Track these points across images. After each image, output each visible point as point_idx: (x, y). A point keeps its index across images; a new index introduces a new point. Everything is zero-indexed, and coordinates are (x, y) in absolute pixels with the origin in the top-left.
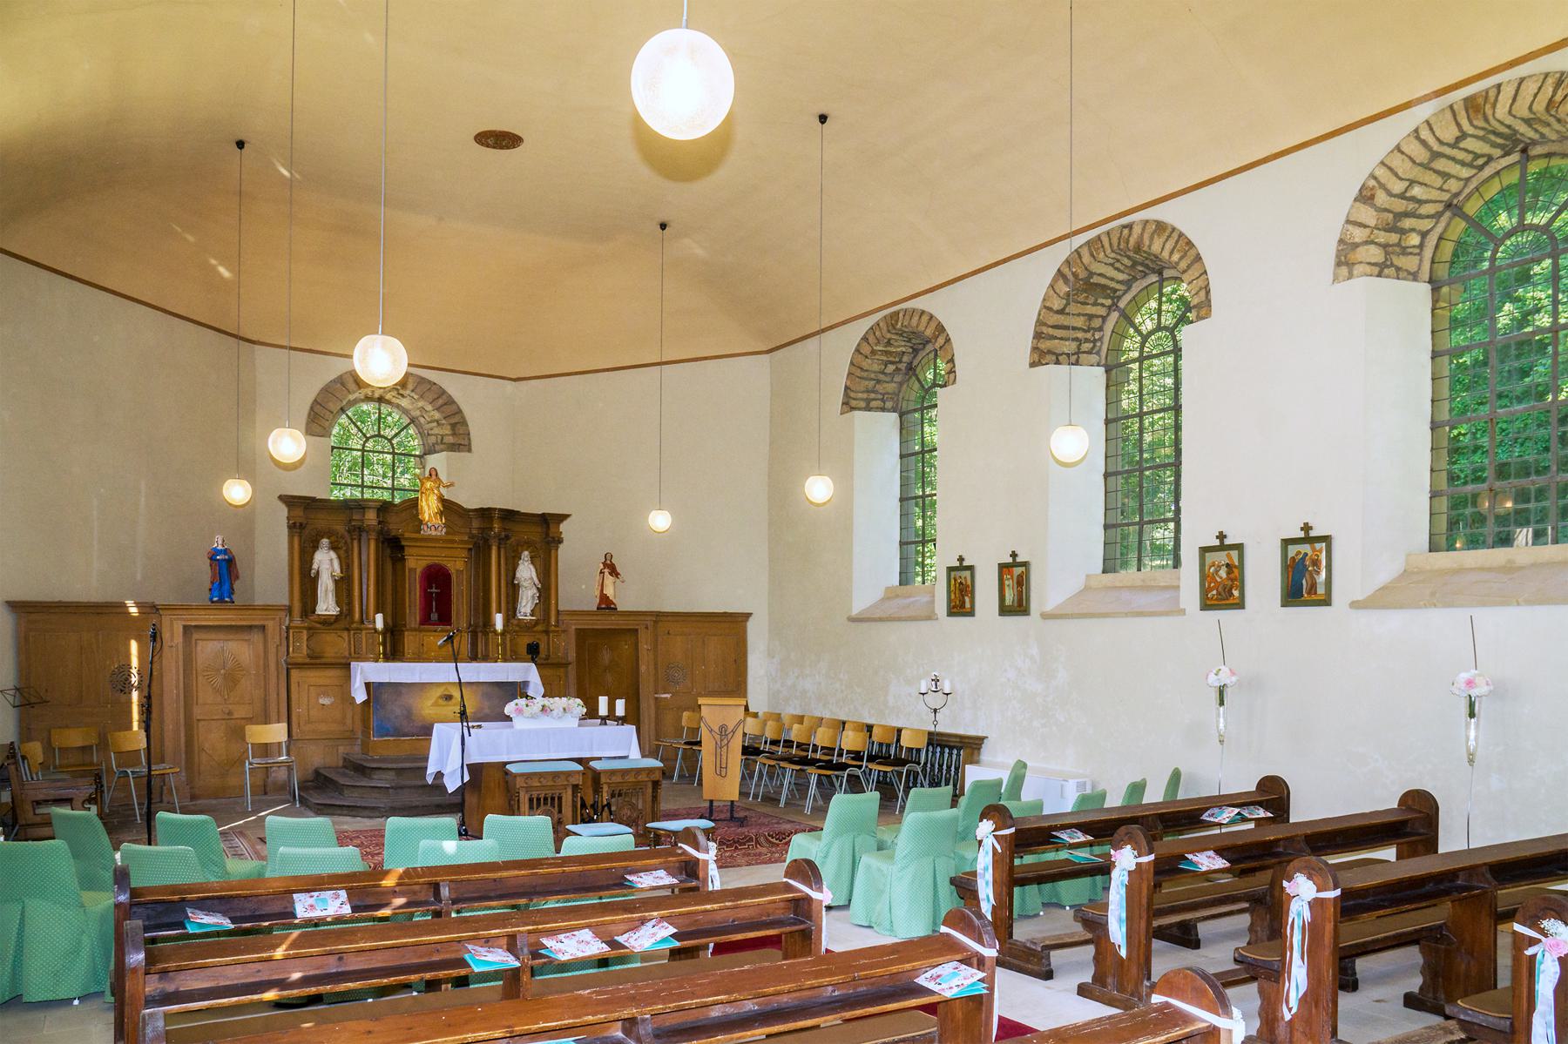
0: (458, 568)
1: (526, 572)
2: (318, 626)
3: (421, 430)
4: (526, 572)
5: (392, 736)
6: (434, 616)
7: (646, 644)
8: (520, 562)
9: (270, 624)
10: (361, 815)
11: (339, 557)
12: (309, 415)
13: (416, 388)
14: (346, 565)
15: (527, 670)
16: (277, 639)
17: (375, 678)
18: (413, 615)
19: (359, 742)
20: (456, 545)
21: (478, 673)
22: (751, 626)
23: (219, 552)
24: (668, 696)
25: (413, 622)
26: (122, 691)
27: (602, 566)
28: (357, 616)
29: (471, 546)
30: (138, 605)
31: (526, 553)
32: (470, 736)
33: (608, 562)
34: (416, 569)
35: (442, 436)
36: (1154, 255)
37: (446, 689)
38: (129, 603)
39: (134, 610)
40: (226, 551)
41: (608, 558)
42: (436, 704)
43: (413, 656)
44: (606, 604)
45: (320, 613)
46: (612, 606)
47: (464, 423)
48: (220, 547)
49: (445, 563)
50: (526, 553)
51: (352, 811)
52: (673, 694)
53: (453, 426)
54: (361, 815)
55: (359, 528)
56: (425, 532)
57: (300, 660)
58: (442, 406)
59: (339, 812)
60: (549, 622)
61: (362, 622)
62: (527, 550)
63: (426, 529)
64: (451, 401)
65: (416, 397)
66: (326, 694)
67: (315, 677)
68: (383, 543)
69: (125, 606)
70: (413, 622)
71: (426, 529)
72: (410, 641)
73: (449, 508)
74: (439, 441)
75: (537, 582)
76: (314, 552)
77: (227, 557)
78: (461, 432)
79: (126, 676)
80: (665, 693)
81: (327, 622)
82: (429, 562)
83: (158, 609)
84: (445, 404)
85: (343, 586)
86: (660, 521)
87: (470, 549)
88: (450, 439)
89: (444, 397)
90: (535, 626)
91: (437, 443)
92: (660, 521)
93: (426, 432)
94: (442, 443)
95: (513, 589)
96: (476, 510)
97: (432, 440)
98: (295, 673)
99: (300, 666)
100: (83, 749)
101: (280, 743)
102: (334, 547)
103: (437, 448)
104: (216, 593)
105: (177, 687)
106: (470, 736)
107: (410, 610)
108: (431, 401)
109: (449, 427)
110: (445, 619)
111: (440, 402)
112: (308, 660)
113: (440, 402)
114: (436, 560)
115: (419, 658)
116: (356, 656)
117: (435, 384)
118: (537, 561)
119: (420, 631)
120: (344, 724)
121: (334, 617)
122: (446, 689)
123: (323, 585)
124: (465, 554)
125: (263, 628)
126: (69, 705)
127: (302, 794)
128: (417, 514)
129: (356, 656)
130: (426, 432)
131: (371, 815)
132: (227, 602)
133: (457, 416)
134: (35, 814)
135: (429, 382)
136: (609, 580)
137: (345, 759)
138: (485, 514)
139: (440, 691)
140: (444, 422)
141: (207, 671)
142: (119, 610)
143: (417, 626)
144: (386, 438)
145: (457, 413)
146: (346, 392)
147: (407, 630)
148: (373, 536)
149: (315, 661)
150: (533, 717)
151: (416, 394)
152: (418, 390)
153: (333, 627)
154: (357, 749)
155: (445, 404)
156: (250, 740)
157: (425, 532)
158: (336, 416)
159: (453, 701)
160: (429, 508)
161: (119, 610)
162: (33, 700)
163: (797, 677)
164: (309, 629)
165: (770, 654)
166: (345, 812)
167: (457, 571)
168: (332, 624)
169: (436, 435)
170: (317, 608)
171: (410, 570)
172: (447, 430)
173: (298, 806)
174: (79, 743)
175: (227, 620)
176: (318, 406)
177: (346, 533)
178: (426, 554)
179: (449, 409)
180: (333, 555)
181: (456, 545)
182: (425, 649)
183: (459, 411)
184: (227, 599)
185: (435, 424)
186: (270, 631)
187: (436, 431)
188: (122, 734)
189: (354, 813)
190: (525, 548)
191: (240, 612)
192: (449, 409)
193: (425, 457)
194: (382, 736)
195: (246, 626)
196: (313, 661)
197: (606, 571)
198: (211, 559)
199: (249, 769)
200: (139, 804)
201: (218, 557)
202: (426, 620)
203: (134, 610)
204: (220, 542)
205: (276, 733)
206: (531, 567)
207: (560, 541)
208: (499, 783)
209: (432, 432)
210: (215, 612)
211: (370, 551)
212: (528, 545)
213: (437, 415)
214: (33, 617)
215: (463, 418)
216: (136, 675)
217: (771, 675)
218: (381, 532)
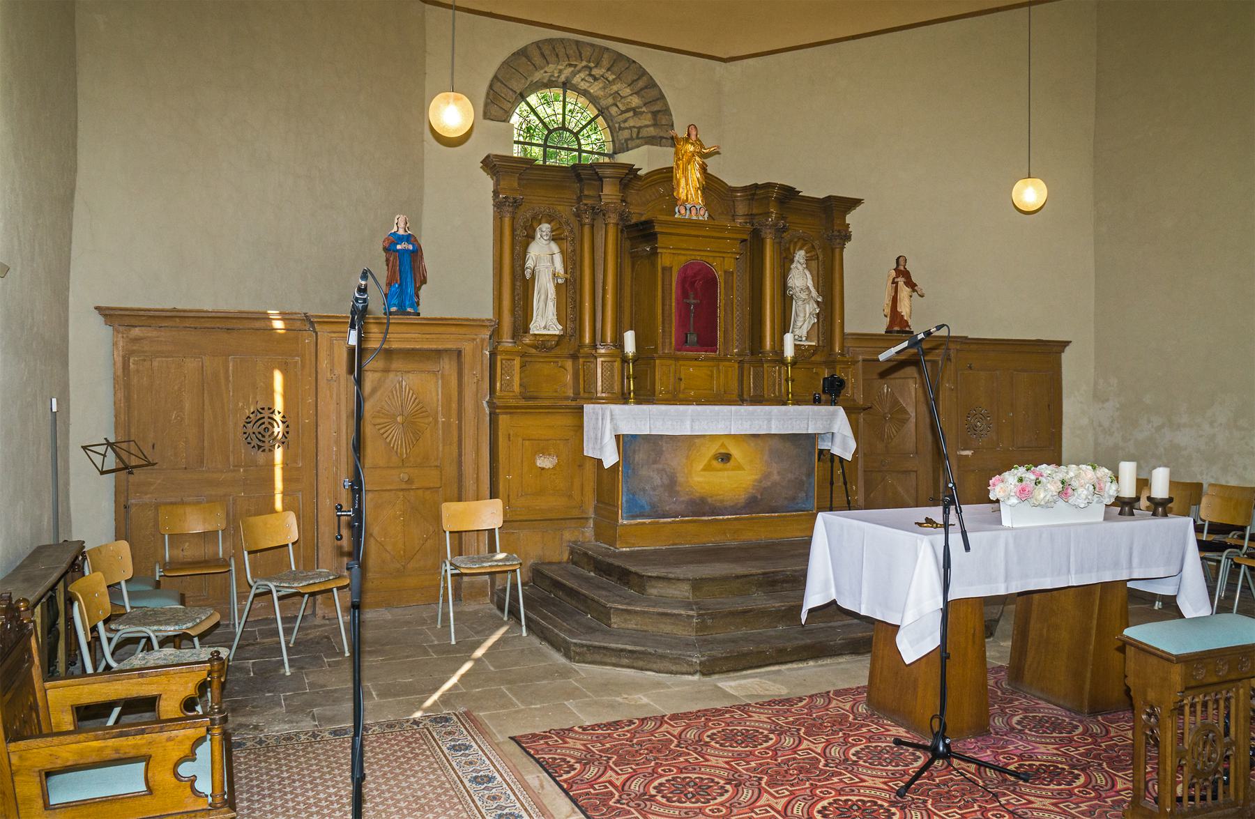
0: (726, 268)
1: (801, 279)
2: (534, 351)
3: (611, 124)
4: (801, 279)
5: (649, 517)
6: (693, 338)
7: (948, 382)
8: (793, 266)
9: (467, 348)
10: (654, 666)
11: (562, 252)
12: (488, 94)
13: (612, 66)
14: (572, 261)
15: (833, 416)
16: (477, 371)
17: (627, 429)
18: (667, 331)
19: (591, 523)
20: (726, 234)
21: (769, 420)
22: (1067, 357)
23: (401, 239)
24: (968, 453)
25: (667, 347)
26: (259, 447)
27: (893, 273)
28: (587, 340)
29: (745, 237)
30: (285, 317)
31: (802, 253)
32: (967, 548)
33: (902, 268)
34: (671, 268)
35: (639, 128)
36: (488, 320)
37: (723, 445)
38: (273, 312)
39: (278, 324)
40: (408, 238)
41: (901, 262)
42: (708, 468)
43: (667, 396)
44: (898, 326)
45: (536, 332)
46: (907, 329)
47: (667, 111)
48: (401, 232)
49: (710, 260)
50: (802, 253)
51: (637, 658)
52: (976, 451)
53: (655, 114)
54: (654, 666)
55: (593, 208)
56: (681, 213)
57: (513, 402)
58: (642, 89)
59: (614, 660)
60: (832, 349)
61: (594, 347)
62: (801, 249)
63: (683, 211)
64: (652, 84)
65: (611, 78)
66: (544, 452)
67: (536, 426)
68: (622, 231)
69: (266, 318)
70: (667, 347)
71: (683, 211)
72: (662, 374)
73: (711, 186)
74: (634, 136)
75: (814, 293)
76: (528, 245)
77: (411, 247)
78: (664, 122)
79: (266, 425)
80: (965, 449)
81: (544, 344)
82: (689, 258)
83: (312, 323)
84: (646, 87)
85: (569, 292)
86: (1030, 194)
87: (744, 241)
88: (652, 131)
89: (645, 78)
90: (813, 354)
91: (631, 139)
92: (1030, 194)
93: (617, 125)
94: (638, 138)
95: (785, 300)
96: (745, 189)
97: (625, 134)
98: (503, 420)
99: (511, 410)
100: (204, 536)
101: (492, 531)
102: (555, 239)
103: (630, 144)
104: (395, 301)
105: (337, 443)
106: (967, 548)
107: (663, 327)
108: (630, 81)
109: (649, 115)
110: (708, 342)
111: (641, 84)
112: (523, 403)
113: (641, 84)
114: (698, 257)
115: (674, 398)
116: (586, 395)
117: (634, 62)
118: (814, 264)
119: (677, 359)
120: (570, 497)
121: (556, 339)
122: (723, 445)
123: (543, 291)
124: (736, 248)
125: (459, 353)
126: (186, 468)
127: (531, 615)
128: (673, 189)
129: (586, 395)
130: (617, 125)
131: (674, 668)
132: (409, 314)
133: (658, 102)
134: (47, 806)
135: (628, 59)
136: (904, 291)
137: (572, 552)
138: (755, 192)
139: (714, 449)
140: (644, 109)
141: (379, 417)
142: (258, 324)
143: (672, 352)
144: (571, 132)
145: (658, 99)
146: (531, 67)
147: (660, 357)
148: (613, 219)
149: (530, 403)
150: (1048, 505)
151: (613, 73)
152: (615, 69)
153: (553, 353)
154: (589, 532)
155: (646, 87)
156: (448, 526)
157: (681, 213)
158: (515, 104)
159: (732, 462)
160: (689, 186)
161: (258, 324)
162: (134, 461)
163: (1159, 429)
164: (523, 355)
165: (1098, 397)
166: (625, 661)
167: (726, 272)
168: (551, 348)
169: (630, 128)
170: (532, 326)
171: (664, 269)
172: (646, 120)
173: (524, 634)
174: (198, 528)
175: (407, 340)
176: (499, 84)
177: (572, 219)
178: (685, 246)
179: (652, 93)
180: (554, 247)
181: (726, 234)
182: (683, 386)
183: (662, 97)
184: (409, 310)
185: (631, 114)
186: (467, 358)
187: (631, 123)
188: (258, 520)
189: (641, 663)
190: (799, 245)
191: (427, 329)
192: (652, 93)
193: (615, 156)
194: (634, 517)
195: (431, 350)
196: (530, 403)
197: (901, 281)
198: (386, 250)
199: (452, 575)
200: (284, 619)
201: (399, 247)
202: (682, 344)
203: (278, 324)
204: (402, 225)
205: (489, 515)
206: (808, 273)
207: (848, 237)
208: (974, 635)
209: (627, 125)
210: (404, 328)
211: (609, 239)
212: (804, 242)
213: (635, 101)
214: (136, 332)
215: (666, 104)
216: (280, 423)
217: (1100, 425)
218: (623, 217)
